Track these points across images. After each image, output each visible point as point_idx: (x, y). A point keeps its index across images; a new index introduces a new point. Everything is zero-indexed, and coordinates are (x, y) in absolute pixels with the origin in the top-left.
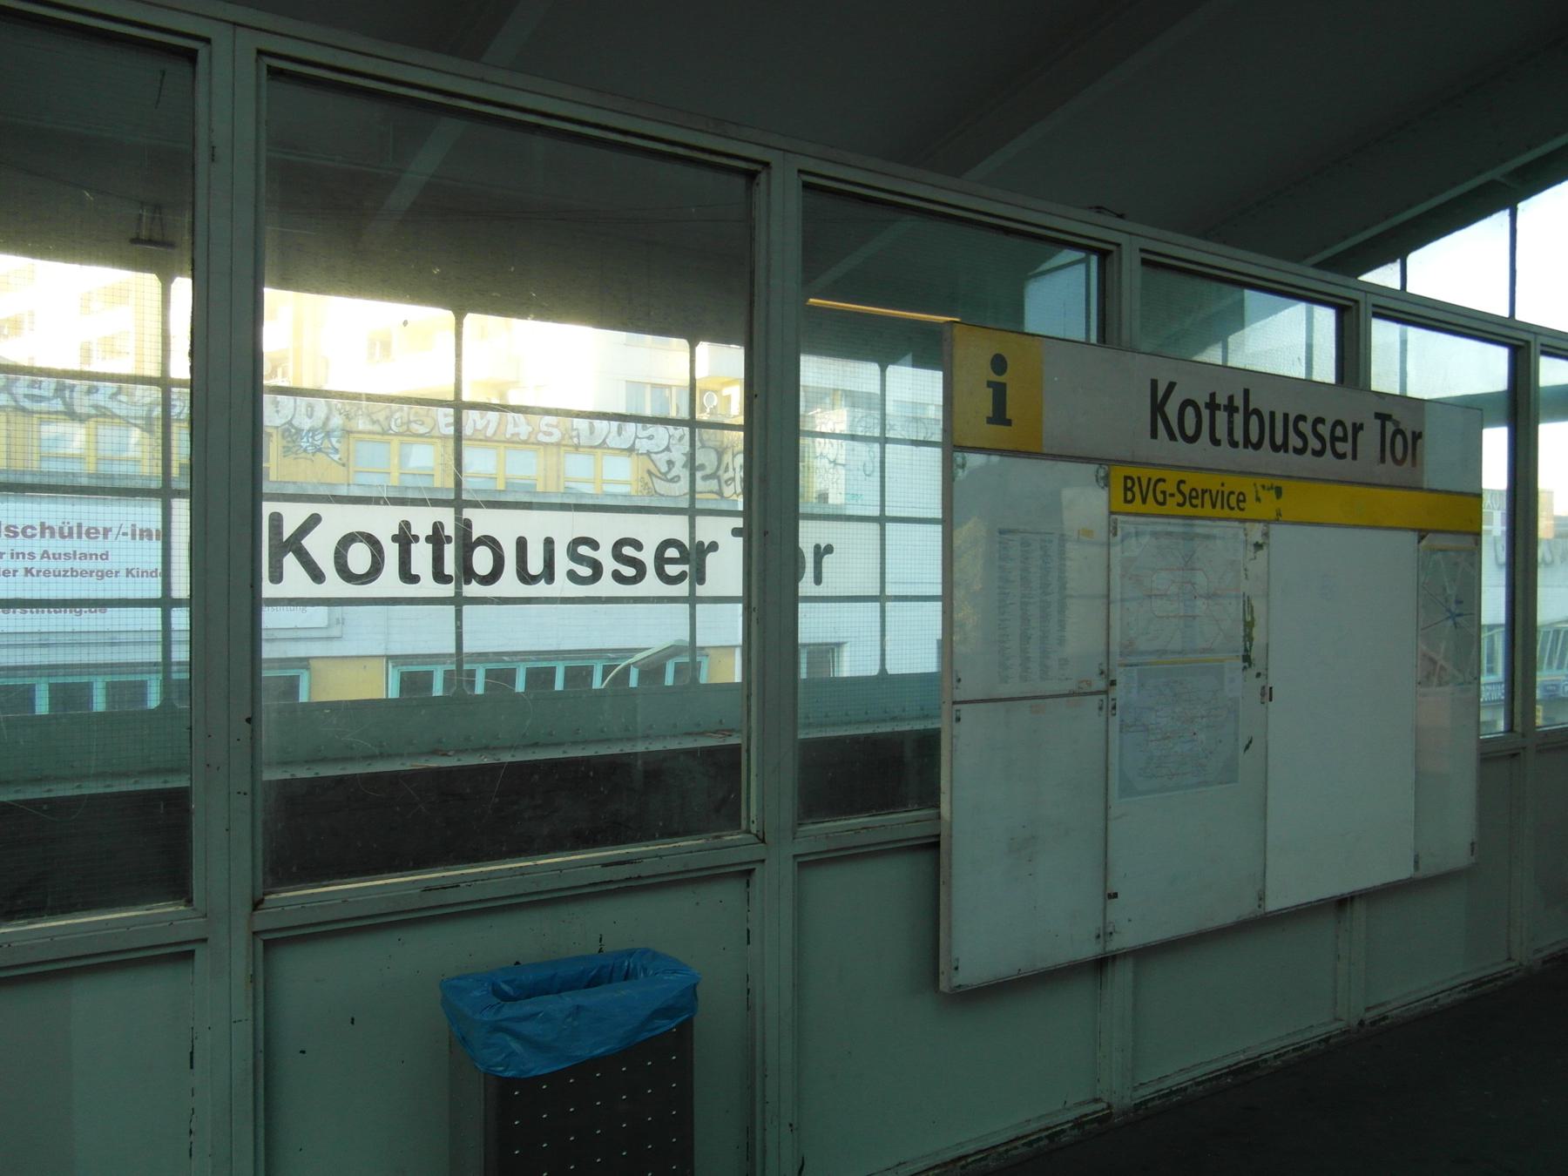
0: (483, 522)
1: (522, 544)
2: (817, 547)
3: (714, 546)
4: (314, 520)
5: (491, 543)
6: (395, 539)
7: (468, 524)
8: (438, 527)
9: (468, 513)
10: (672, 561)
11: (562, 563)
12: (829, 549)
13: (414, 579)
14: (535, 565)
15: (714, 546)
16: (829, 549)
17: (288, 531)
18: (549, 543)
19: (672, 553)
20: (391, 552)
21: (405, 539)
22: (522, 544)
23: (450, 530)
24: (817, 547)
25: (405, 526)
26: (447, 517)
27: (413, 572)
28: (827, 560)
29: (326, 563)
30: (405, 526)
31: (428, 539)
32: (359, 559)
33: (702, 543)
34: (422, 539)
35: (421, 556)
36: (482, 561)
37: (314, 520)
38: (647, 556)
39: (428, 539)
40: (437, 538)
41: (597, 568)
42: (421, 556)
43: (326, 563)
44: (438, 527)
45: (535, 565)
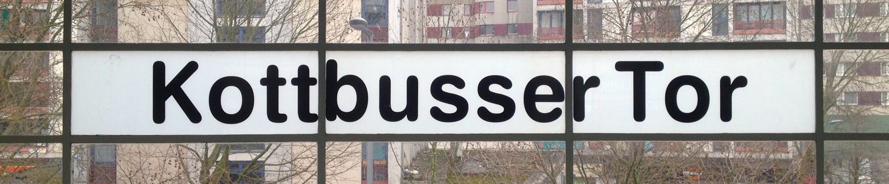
0: (347, 64)
1: (385, 83)
2: (725, 81)
3: (594, 82)
4: (192, 68)
5: (355, 81)
6: (263, 82)
7: (333, 65)
8: (304, 70)
9: (330, 56)
10: (545, 98)
11: (426, 101)
12: (741, 82)
13: (282, 118)
14: (398, 103)
15: (594, 82)
16: (741, 82)
17: (169, 78)
18: (412, 83)
19: (544, 90)
20: (260, 94)
21: (273, 80)
22: (385, 83)
23: (314, 73)
24: (725, 81)
25: (273, 70)
26: (311, 60)
27: (281, 111)
28: (737, 95)
29: (202, 104)
30: (273, 70)
31: (294, 82)
32: (232, 100)
33: (579, 79)
34: (289, 82)
35: (288, 97)
36: (346, 98)
37: (192, 68)
38: (517, 94)
39: (294, 82)
40: (303, 80)
41: (462, 107)
42: (288, 97)
43: (202, 104)
44: (304, 70)
45: (398, 103)
